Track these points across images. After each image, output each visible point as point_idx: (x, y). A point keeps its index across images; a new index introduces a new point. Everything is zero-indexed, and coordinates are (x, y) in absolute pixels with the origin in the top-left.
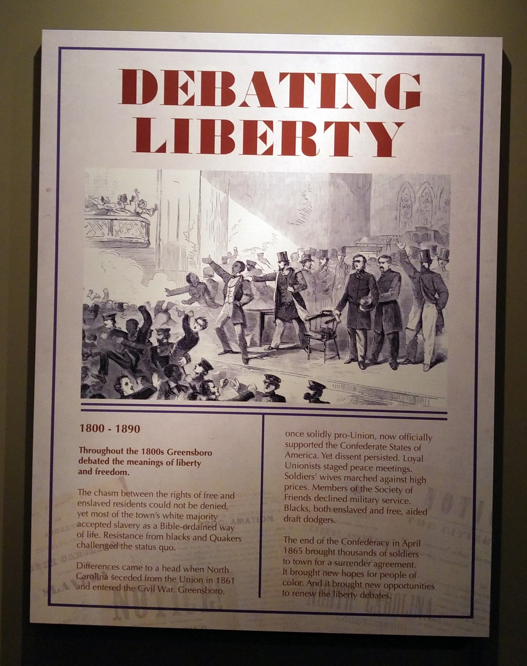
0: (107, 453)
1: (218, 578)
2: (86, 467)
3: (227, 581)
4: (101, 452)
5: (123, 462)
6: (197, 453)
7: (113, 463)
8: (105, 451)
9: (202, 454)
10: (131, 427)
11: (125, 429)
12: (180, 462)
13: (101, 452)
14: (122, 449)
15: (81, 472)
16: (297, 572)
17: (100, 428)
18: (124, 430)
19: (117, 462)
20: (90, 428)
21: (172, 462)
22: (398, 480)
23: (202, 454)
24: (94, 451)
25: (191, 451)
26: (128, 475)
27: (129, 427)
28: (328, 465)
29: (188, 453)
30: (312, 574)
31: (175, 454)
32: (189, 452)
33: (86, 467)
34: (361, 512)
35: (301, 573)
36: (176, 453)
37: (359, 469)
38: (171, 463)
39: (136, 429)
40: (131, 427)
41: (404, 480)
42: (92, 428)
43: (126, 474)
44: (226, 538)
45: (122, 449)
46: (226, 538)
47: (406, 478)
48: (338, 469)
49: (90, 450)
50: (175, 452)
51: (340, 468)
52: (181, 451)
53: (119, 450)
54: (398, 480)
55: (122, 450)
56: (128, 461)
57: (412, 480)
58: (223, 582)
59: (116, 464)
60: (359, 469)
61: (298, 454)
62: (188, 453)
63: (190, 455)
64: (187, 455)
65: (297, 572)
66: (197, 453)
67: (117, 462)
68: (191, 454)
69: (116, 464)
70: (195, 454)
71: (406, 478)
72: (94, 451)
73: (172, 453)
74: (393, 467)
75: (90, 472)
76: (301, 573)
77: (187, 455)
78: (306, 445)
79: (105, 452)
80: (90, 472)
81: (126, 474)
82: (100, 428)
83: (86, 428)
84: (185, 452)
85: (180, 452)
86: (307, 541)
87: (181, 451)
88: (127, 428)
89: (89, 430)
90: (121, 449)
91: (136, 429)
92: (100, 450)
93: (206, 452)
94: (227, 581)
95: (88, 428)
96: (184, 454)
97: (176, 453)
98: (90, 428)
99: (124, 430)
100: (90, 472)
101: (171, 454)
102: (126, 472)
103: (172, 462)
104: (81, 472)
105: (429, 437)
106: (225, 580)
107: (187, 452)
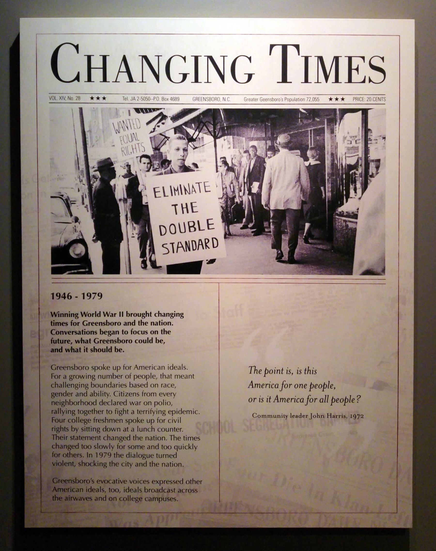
0: (146, 316)
2: (58, 346)
4: (142, 315)
5: (148, 323)
6: (108, 324)
8: (144, 314)
9: (112, 324)
13: (142, 315)
15: (53, 351)
19: (142, 323)
23: (112, 324)
24: (135, 315)
25: (103, 322)
26: (172, 325)
28: (74, 436)
29: (101, 324)
32: (102, 323)
33: (58, 346)
37: (133, 491)
41: (173, 490)
43: (170, 325)
44: (103, 367)
46: (103, 367)
47: (174, 489)
48: (71, 448)
49: (131, 314)
50: (89, 323)
51: (73, 447)
52: (95, 323)
56: (151, 323)
57: (256, 371)
59: (141, 325)
60: (133, 491)
61: (59, 422)
62: (101, 324)
64: (99, 325)
66: (108, 324)
67: (142, 323)
69: (141, 325)
70: (118, 342)
72: (135, 315)
73: (98, 342)
74: (92, 410)
75: (61, 351)
77: (99, 325)
78: (80, 368)
79: (145, 316)
80: (61, 351)
81: (170, 325)
85: (94, 323)
86: (61, 394)
87: (95, 323)
92: (140, 314)
96: (108, 342)
100: (60, 350)
102: (170, 323)
104: (53, 351)
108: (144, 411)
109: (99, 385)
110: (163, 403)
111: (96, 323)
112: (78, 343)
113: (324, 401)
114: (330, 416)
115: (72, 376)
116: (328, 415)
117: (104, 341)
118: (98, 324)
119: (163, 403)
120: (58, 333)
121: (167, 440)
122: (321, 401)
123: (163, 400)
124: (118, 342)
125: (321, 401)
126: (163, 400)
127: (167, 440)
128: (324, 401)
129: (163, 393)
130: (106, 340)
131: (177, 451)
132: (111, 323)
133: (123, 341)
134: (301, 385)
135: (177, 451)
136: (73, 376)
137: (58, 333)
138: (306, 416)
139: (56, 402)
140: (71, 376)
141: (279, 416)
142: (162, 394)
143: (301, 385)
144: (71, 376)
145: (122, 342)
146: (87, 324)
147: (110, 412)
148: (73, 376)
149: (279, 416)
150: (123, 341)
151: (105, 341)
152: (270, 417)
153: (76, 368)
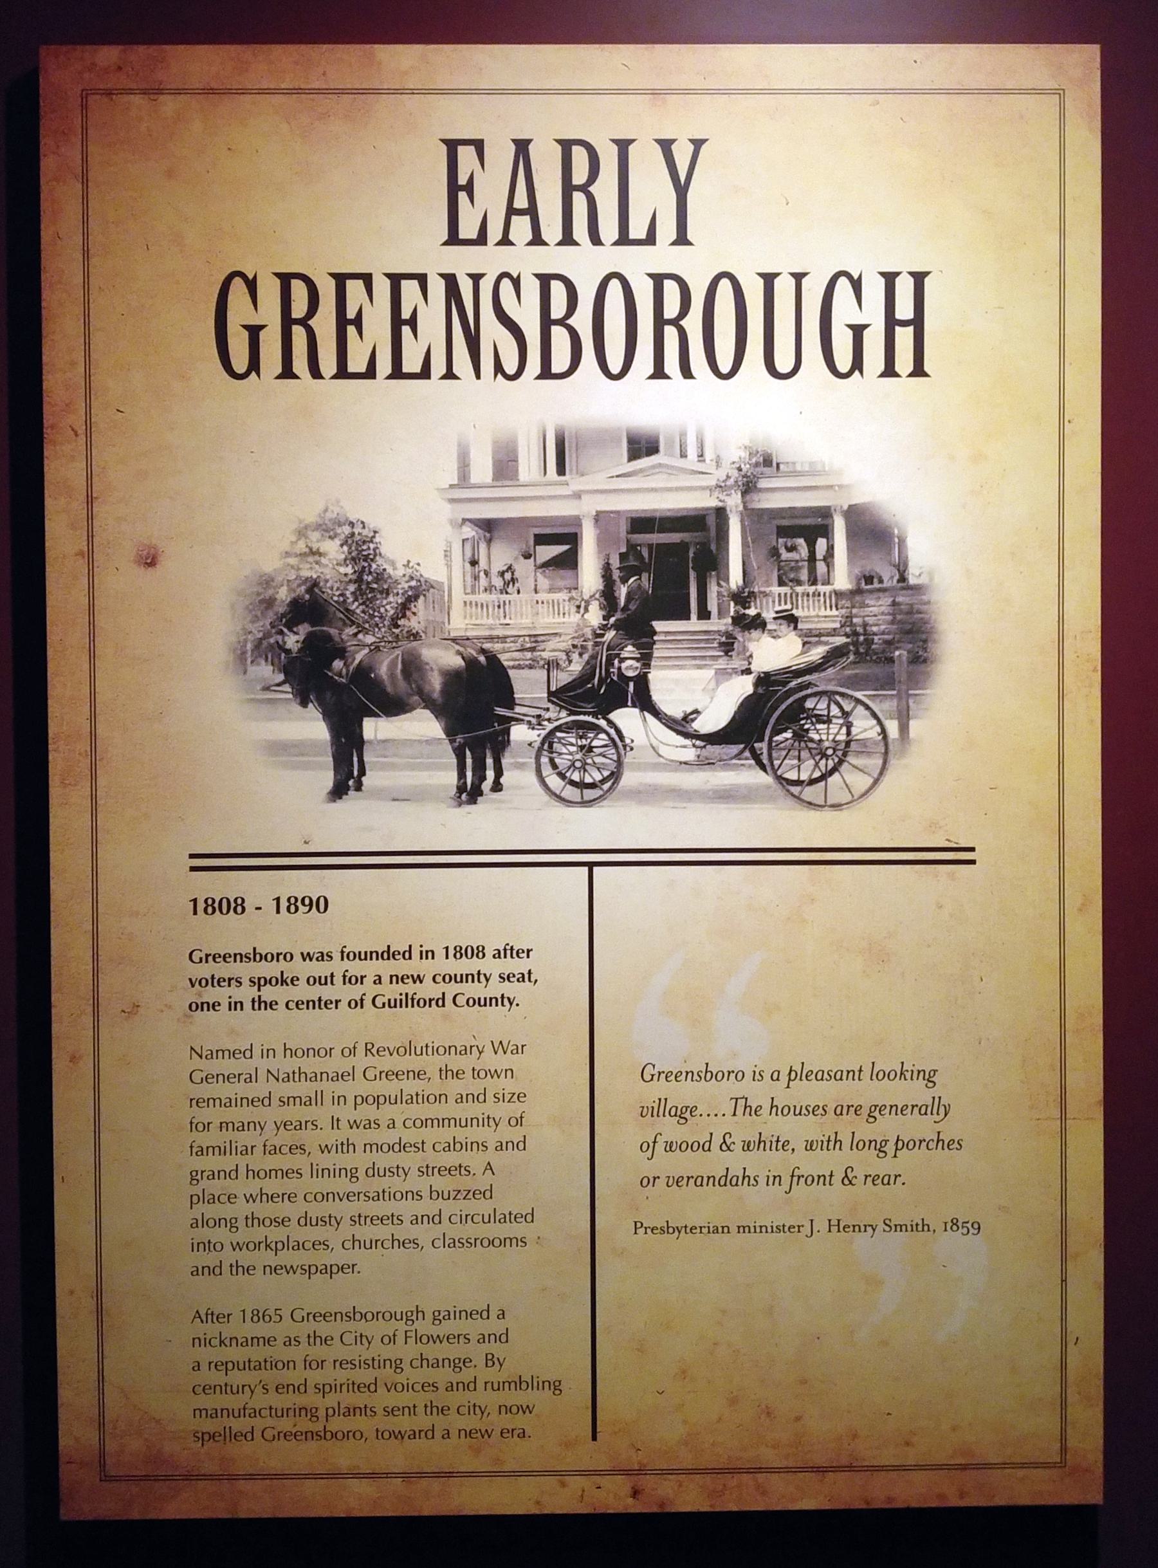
1: (244, 1311)
3: (264, 1316)
6: (258, 957)
7: (253, 1008)
10: (307, 901)
11: (294, 904)
12: (401, 1000)
14: (332, 974)
16: (380, 1316)
17: (237, 906)
18: (293, 909)
20: (214, 906)
21: (362, 1000)
22: (475, 1145)
25: (244, 954)
27: (303, 899)
29: (238, 957)
30: (414, 1318)
31: (207, 961)
34: (322, 1318)
35: (387, 1316)
36: (210, 958)
38: (359, 1002)
39: (319, 905)
40: (307, 901)
42: (463, 951)
45: (332, 974)
50: (207, 956)
53: (326, 977)
54: (475, 1145)
55: (332, 975)
58: (255, 1318)
62: (238, 957)
63: (241, 961)
64: (235, 961)
65: (380, 1316)
66: (258, 957)
68: (244, 959)
69: (260, 1008)
70: (255, 960)
71: (423, 1143)
73: (201, 959)
76: (387, 1316)
82: (237, 906)
83: (454, 952)
84: (224, 981)
85: (220, 956)
88: (299, 904)
89: (458, 955)
90: (329, 975)
91: (319, 905)
93: (278, 955)
94: (264, 1316)
95: (456, 952)
96: (228, 960)
97: (210, 958)
98: (214, 906)
99: (293, 909)
101: (198, 961)
103: (362, 1000)
105: (498, 1359)
106: (261, 1315)
107: (235, 955)
108: (459, 1336)
109: (256, 1177)
110: (530, 1385)
111: (225, 955)
112: (418, 982)
113: (929, 1112)
114: (837, 1227)
115: (197, 1171)
116: (832, 1223)
117: (217, 956)
118: (232, 959)
119: (530, 1385)
120: (471, 1002)
121: (359, 1272)
122: (838, 1112)
123: (532, 1377)
124: (255, 960)
125: (838, 1112)
126: (532, 1377)
127: (359, 1272)
128: (929, 1112)
129: (388, 1048)
130: (222, 955)
131: (325, 1427)
132: (272, 961)
133: (269, 957)
134: (712, 1179)
135: (325, 1427)
136: (199, 1173)
137: (471, 1002)
138: (797, 1228)
139: (471, 1431)
140: (194, 1174)
141: (764, 1229)
142: (385, 1050)
143: (712, 1179)
144: (194, 1174)
145: (266, 960)
146: (201, 959)
147: (218, 1247)
148: (199, 1173)
149: (764, 1229)
150: (269, 957)
151: (220, 956)
152: (744, 1232)
153: (358, 1316)
